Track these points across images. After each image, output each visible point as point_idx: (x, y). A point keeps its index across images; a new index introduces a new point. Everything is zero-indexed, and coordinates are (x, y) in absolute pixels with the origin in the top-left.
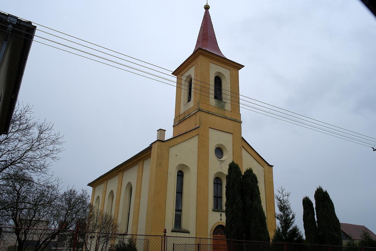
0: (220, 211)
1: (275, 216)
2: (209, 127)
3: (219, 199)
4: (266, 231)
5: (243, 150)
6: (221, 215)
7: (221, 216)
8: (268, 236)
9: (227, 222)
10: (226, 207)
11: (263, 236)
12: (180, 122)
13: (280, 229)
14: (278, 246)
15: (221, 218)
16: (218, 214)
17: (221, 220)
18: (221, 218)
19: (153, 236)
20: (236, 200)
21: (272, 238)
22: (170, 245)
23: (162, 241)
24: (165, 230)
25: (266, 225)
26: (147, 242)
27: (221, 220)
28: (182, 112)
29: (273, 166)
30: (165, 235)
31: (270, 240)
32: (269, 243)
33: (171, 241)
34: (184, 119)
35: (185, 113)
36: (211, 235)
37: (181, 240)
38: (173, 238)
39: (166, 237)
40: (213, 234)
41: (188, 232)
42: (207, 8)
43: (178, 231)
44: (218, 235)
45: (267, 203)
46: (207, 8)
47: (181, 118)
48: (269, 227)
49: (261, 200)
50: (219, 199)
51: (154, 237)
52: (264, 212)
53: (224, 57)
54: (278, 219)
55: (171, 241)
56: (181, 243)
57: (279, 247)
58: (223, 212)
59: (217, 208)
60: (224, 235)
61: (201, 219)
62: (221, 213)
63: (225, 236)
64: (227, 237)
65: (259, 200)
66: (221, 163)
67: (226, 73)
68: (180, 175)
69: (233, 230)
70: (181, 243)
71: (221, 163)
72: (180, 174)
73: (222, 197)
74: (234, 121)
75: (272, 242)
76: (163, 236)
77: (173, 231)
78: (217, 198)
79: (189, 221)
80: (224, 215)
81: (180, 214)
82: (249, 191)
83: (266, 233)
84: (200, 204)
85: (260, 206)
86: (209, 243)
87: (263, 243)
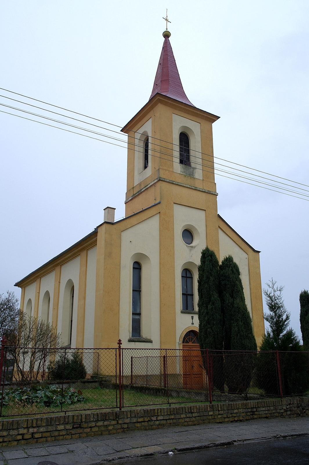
2: (174, 203)
3: (189, 297)
4: (252, 336)
5: (220, 231)
6: (192, 318)
7: (192, 319)
10: (199, 308)
12: (134, 197)
15: (192, 321)
17: (193, 324)
18: (192, 321)
20: (212, 297)
21: (261, 345)
22: (126, 360)
23: (116, 355)
24: (120, 341)
26: (156, 384)
27: (193, 324)
28: (136, 183)
29: (260, 252)
30: (120, 347)
31: (257, 348)
34: (140, 193)
35: (140, 184)
36: (180, 344)
39: (121, 349)
40: (183, 342)
41: (150, 341)
42: (167, 35)
44: (189, 343)
45: (252, 300)
46: (167, 35)
47: (136, 191)
48: (255, 331)
49: (244, 297)
53: (191, 105)
54: (267, 321)
55: (127, 355)
58: (195, 313)
59: (187, 308)
60: (197, 343)
61: (167, 324)
62: (192, 315)
63: (198, 344)
64: (202, 346)
65: (241, 296)
66: (190, 250)
67: (195, 127)
68: (137, 267)
69: (209, 337)
71: (190, 250)
72: (137, 266)
73: (194, 294)
74: (207, 193)
76: (156, 420)
77: (130, 341)
78: (187, 296)
79: (151, 327)
80: (196, 317)
82: (229, 286)
83: (252, 339)
84: (165, 304)
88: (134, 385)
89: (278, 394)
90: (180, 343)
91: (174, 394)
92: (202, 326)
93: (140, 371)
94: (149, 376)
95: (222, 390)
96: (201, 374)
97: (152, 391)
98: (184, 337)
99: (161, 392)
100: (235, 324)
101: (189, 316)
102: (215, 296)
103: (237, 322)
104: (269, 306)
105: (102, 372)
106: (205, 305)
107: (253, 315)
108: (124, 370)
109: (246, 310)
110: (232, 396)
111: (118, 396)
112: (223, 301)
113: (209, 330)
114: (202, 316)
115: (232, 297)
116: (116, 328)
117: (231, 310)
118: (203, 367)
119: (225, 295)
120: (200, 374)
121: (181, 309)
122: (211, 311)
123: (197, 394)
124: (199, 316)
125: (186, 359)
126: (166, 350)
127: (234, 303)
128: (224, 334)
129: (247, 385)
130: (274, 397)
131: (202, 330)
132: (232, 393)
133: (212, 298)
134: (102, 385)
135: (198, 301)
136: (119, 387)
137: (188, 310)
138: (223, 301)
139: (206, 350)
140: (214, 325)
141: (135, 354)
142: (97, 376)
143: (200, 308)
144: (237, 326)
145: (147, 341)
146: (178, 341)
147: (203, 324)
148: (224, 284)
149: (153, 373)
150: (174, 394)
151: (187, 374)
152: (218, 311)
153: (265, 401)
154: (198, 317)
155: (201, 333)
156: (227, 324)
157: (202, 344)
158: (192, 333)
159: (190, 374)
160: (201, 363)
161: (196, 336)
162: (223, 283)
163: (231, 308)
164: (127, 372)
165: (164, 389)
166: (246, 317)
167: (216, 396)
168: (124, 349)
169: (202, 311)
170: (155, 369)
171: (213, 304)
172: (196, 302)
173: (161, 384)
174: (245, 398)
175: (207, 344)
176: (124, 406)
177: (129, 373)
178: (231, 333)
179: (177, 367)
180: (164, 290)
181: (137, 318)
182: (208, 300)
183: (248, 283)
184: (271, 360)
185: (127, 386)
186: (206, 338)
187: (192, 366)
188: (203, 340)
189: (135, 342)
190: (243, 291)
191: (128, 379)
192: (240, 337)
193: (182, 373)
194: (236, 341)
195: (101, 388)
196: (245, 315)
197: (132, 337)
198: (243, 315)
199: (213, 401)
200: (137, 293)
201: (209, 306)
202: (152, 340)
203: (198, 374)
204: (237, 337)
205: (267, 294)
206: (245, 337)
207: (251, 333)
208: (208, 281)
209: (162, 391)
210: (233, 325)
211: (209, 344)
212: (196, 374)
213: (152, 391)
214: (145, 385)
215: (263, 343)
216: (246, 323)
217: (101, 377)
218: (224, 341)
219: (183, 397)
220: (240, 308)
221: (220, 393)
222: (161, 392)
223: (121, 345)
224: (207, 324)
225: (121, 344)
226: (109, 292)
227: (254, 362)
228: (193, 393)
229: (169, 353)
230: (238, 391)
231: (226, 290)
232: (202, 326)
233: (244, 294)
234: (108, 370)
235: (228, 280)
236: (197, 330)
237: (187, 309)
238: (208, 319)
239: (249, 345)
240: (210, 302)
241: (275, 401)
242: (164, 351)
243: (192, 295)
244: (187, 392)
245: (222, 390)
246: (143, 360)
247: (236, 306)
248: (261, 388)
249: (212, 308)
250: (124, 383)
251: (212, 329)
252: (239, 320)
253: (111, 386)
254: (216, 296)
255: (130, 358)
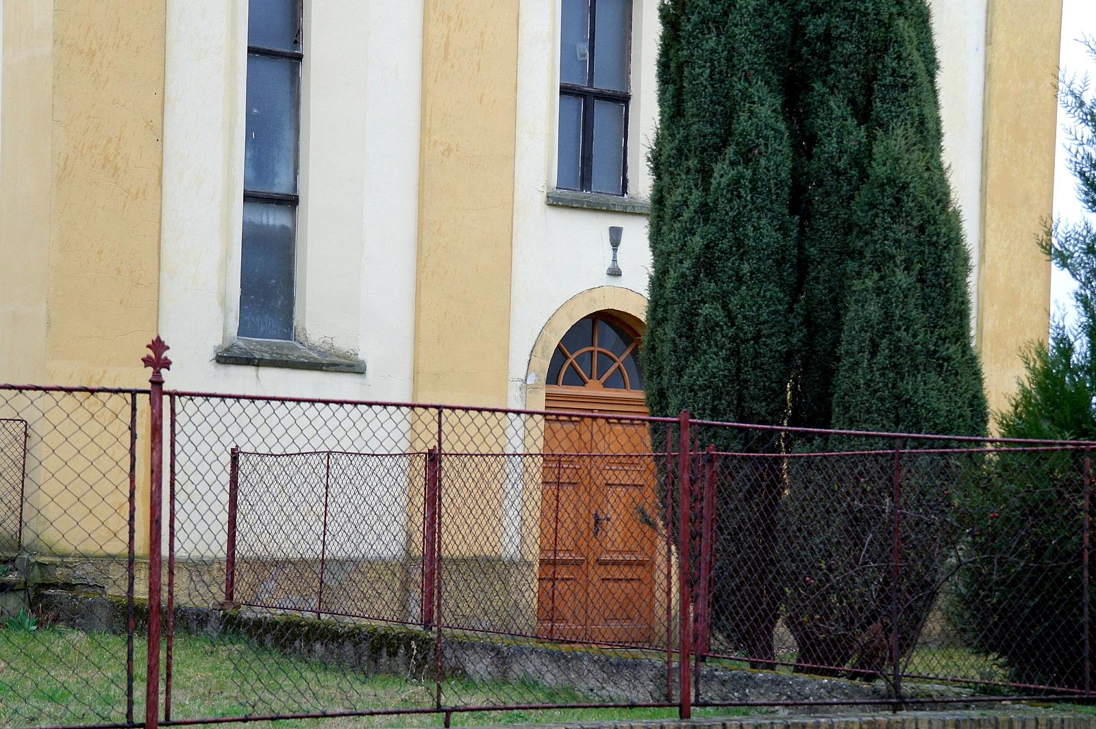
0: (613, 202)
1: (1047, 248)
3: (603, 113)
4: (964, 352)
6: (615, 237)
7: (615, 243)
8: (975, 397)
9: (662, 286)
10: (659, 177)
11: (934, 393)
13: (1071, 345)
14: (1046, 467)
15: (614, 260)
16: (595, 227)
17: (615, 273)
18: (614, 260)
19: (61, 389)
20: (744, 116)
21: (1007, 408)
22: (196, 458)
23: (132, 428)
24: (158, 346)
25: (962, 314)
26: (376, 609)
27: (615, 273)
30: (157, 383)
31: (985, 422)
32: (978, 443)
33: (205, 428)
36: (535, 388)
37: (288, 421)
38: (301, 441)
39: (166, 398)
40: (552, 379)
41: (354, 367)
43: (267, 357)
44: (584, 383)
45: (993, 143)
48: (988, 326)
49: (938, 121)
50: (603, 113)
51: (68, 401)
52: (956, 214)
54: (1064, 265)
55: (205, 428)
56: (286, 441)
57: (1052, 470)
58: (630, 211)
59: (585, 177)
61: (454, 267)
63: (639, 395)
64: (659, 401)
65: (921, 115)
69: (705, 352)
70: (286, 441)
75: (997, 436)
76: (138, 396)
77: (226, 358)
78: (590, 101)
79: (355, 279)
80: (637, 233)
81: (289, 224)
82: (850, 48)
83: (963, 371)
84: (449, 150)
85: (928, 169)
86: (515, 444)
87: (932, 443)
88: (247, 614)
89: (1081, 687)
90: (528, 383)
91: (479, 666)
92: (670, 284)
93: (282, 527)
94: (341, 563)
95: (756, 646)
96: (647, 564)
97: (348, 647)
98: (559, 346)
99: (402, 651)
100: (869, 283)
101: (599, 225)
102: (763, 109)
103: (879, 270)
104: (1082, 174)
105: (50, 535)
106: (692, 163)
107: (989, 233)
108: (180, 516)
109: (939, 202)
110: (816, 685)
111: (141, 670)
112: (804, 141)
113: (705, 310)
114: (671, 230)
115: (863, 114)
116: (145, 278)
117: (852, 197)
118: (660, 524)
119: (821, 102)
120: (641, 564)
121: (548, 182)
122: (730, 201)
123: (614, 669)
124: (651, 225)
125: (560, 472)
126: (440, 414)
127: (870, 156)
128: (795, 340)
129: (907, 643)
130: (1057, 701)
131: (666, 311)
132: (815, 671)
133: (743, 123)
134: (47, 607)
135: (652, 136)
136: (151, 621)
137: (589, 188)
138: (804, 141)
139: (678, 422)
140: (740, 280)
141: (259, 431)
142: (14, 555)
143: (666, 178)
144: (879, 291)
145: (335, 365)
146: (518, 367)
147: (672, 272)
148: (818, 38)
149: (364, 547)
150: (479, 666)
151: (565, 563)
152: (772, 203)
153: (998, 714)
154: (647, 230)
155: (659, 324)
156: (816, 279)
157: (662, 394)
158: (609, 331)
159: (577, 564)
160: (651, 500)
161: (627, 345)
162: (815, 26)
163: (850, 184)
164: (198, 533)
165: (416, 637)
166: (934, 244)
167: (723, 683)
168: (181, 395)
169: (672, 199)
170: (378, 525)
171: (747, 156)
172: (643, 140)
173: (404, 606)
174: (890, 697)
175: (691, 390)
176: (172, 719)
177: (215, 548)
178: (841, 330)
179: (504, 521)
180: (445, 58)
181: (271, 222)
182: (714, 134)
183: (975, 33)
184: (1060, 494)
185: (202, 618)
186: (686, 359)
187: (597, 521)
188: (667, 369)
189: (258, 366)
190: (932, 82)
191: (206, 578)
192: (891, 357)
193: (533, 553)
194: (867, 384)
195: (40, 624)
196: (930, 229)
197: (242, 332)
198: (922, 229)
199: (697, 704)
200: (275, 71)
201: (718, 168)
202: (361, 357)
203: (629, 563)
204: (873, 354)
205: (1082, 104)
206: (921, 359)
207: (961, 336)
208: (726, 14)
209: (408, 648)
210: (857, 285)
211: (700, 394)
212: (615, 563)
213: (348, 647)
214: (308, 615)
215: (1025, 397)
216: (937, 275)
217: (41, 565)
218: (795, 379)
219: (530, 684)
220: (905, 187)
221: (746, 666)
222: (402, 651)
223: (163, 371)
224: (697, 277)
225: (167, 364)
226: (92, 54)
227: (956, 502)
228: (591, 660)
229: (459, 429)
230: (853, 660)
231: (830, 71)
232: (670, 284)
233: (936, 103)
234: (90, 524)
235: (845, 9)
236: (638, 307)
237: (585, 181)
238: (707, 247)
239: (944, 407)
240: (725, 143)
241: (1063, 721)
242: (429, 416)
243: (622, 99)
244: (556, 658)
245: (756, 646)
246: (303, 476)
247: (879, 170)
248: (983, 649)
249: (736, 182)
250: (181, 599)
251: (724, 306)
252: (892, 257)
253: (102, 613)
254: (764, 111)
255: (227, 459)
